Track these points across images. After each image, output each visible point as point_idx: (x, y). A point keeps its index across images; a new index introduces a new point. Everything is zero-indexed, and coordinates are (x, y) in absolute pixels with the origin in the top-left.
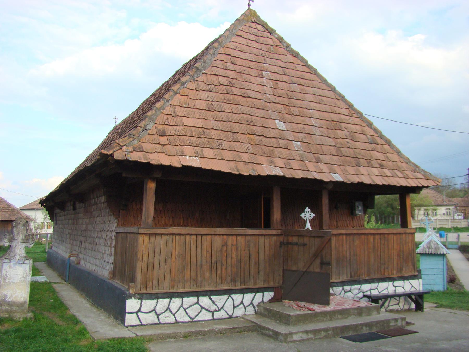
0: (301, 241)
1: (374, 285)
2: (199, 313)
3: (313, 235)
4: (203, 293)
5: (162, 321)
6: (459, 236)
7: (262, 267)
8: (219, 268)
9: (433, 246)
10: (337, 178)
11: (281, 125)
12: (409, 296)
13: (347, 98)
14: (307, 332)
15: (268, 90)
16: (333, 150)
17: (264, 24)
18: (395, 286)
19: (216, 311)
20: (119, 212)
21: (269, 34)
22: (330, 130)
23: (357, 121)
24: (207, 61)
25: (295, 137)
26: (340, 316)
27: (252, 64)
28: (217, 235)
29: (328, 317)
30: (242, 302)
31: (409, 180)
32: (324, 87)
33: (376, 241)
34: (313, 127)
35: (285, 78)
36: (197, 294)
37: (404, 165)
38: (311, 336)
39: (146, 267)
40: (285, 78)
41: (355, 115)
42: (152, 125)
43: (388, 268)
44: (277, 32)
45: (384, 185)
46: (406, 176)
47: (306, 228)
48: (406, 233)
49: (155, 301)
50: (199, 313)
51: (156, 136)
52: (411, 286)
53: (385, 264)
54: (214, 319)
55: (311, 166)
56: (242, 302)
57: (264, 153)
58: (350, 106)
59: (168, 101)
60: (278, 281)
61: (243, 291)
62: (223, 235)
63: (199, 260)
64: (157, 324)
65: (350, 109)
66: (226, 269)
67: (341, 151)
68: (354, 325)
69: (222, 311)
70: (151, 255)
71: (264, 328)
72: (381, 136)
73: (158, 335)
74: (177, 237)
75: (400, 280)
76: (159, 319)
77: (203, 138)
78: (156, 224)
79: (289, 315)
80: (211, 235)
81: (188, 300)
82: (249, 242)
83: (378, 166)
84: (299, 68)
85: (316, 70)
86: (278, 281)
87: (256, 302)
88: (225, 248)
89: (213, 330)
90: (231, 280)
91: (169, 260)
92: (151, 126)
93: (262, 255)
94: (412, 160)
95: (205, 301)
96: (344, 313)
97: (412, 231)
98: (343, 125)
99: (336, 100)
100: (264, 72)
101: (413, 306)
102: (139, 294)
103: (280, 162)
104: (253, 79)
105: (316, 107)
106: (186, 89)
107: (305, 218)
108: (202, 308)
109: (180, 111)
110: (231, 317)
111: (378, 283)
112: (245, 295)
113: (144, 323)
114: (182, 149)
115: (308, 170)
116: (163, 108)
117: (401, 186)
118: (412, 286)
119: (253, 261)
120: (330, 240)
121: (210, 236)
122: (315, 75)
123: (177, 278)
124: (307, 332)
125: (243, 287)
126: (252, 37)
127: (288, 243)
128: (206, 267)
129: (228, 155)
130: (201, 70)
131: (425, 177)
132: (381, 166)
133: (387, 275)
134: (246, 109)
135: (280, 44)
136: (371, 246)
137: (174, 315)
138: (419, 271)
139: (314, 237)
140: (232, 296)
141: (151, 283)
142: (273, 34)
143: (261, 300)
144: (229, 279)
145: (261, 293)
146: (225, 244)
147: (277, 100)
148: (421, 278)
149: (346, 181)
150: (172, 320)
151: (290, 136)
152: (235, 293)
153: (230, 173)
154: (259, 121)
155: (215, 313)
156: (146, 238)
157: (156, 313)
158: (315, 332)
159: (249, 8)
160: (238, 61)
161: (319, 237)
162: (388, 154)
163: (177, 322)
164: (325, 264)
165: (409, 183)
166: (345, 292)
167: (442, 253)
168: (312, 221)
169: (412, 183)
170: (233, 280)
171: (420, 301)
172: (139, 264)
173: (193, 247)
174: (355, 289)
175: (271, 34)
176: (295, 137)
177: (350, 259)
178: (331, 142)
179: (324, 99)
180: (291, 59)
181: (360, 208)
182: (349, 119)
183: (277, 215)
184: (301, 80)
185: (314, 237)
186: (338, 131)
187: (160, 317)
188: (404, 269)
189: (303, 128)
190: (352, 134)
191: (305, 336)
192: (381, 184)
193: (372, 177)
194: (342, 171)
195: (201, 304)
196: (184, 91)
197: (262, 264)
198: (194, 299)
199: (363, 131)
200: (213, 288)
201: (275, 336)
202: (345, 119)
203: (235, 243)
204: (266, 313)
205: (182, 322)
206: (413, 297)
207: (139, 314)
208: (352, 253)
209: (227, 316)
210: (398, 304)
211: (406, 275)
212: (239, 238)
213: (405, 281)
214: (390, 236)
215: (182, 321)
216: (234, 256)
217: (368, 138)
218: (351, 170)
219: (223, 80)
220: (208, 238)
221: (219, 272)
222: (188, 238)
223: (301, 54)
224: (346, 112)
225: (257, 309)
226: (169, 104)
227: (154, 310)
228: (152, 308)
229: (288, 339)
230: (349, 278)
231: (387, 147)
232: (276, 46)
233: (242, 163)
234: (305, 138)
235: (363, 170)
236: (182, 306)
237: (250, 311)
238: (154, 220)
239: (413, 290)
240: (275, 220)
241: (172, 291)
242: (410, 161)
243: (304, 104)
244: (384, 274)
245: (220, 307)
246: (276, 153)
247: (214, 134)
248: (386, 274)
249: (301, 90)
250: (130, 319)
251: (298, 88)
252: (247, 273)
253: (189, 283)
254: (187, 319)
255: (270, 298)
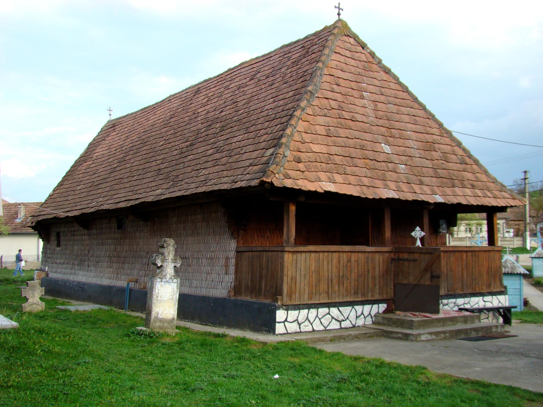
0: (411, 257)
1: (467, 300)
2: (330, 322)
3: (423, 251)
4: (333, 304)
5: (302, 330)
6: (517, 257)
7: (377, 282)
8: (345, 282)
9: (508, 264)
10: (439, 199)
11: (387, 149)
12: (496, 310)
13: (437, 117)
14: (431, 334)
15: (370, 112)
16: (431, 172)
17: (355, 37)
18: (484, 301)
19: (343, 321)
20: (239, 231)
21: (361, 48)
22: (426, 152)
23: (447, 140)
24: (318, 84)
25: (399, 160)
26: (450, 323)
27: (353, 85)
28: (343, 252)
29: (442, 324)
30: (362, 313)
31: (498, 200)
32: (416, 106)
33: (468, 258)
34: (412, 150)
35: (382, 98)
36: (328, 305)
37: (492, 185)
38: (434, 337)
39: (291, 281)
40: (382, 98)
41: (445, 135)
42: (289, 152)
43: (478, 284)
44: (368, 46)
45: (478, 205)
46: (495, 196)
47: (417, 245)
48: (493, 251)
49: (298, 311)
50: (330, 322)
51: (294, 163)
52: (498, 301)
53: (476, 280)
54: (341, 328)
55: (416, 188)
56: (362, 313)
57: (378, 176)
58: (440, 125)
59: (295, 128)
60: (391, 294)
61: (363, 303)
62: (348, 252)
63: (330, 274)
64: (299, 332)
65: (441, 129)
66: (350, 283)
67: (437, 173)
68: (465, 329)
69: (348, 321)
70: (294, 270)
71: (391, 332)
72: (470, 156)
73: (311, 339)
74: (313, 255)
75: (489, 296)
76: (300, 328)
77: (329, 164)
78: (297, 242)
79: (412, 321)
80: (339, 252)
81: (323, 311)
82: (368, 258)
83: (471, 187)
84: (393, 86)
85: (407, 88)
86: (391, 294)
87: (373, 313)
88: (349, 264)
89: (350, 335)
90: (354, 293)
91: (308, 275)
92: (288, 153)
93: (377, 270)
94: (499, 179)
95: (334, 311)
96: (453, 320)
97: (499, 249)
98: (436, 146)
99: (427, 120)
100: (364, 93)
101: (501, 320)
102: (285, 306)
103: (392, 185)
104: (357, 101)
105: (412, 128)
106: (306, 115)
107: (416, 236)
108: (333, 318)
109: (307, 138)
110: (354, 326)
111: (470, 297)
112: (365, 306)
113: (289, 332)
114: (318, 175)
115: (415, 193)
116: (292, 135)
117: (493, 206)
118: (500, 302)
119: (370, 276)
120: (439, 256)
121: (338, 253)
122: (406, 94)
123: (314, 292)
124: (431, 334)
125: (364, 299)
126: (348, 54)
127: (399, 259)
128: (335, 281)
129: (352, 179)
130: (314, 94)
131: (512, 196)
132: (473, 187)
133: (477, 290)
134: (357, 134)
135: (372, 60)
136: (464, 262)
137: (312, 324)
138: (505, 287)
139: (425, 253)
140: (355, 307)
141: (294, 296)
142: (365, 48)
143: (377, 311)
144: (352, 291)
145: (377, 305)
146: (349, 261)
147: (380, 122)
148: (507, 294)
149: (447, 202)
150: (309, 328)
151: (395, 159)
152: (357, 305)
153: (359, 197)
154: (369, 145)
155: (342, 323)
156: (290, 255)
157: (298, 322)
158: (437, 334)
159: (339, 17)
160: (341, 82)
161: (428, 253)
162: (477, 174)
163: (314, 330)
164: (435, 277)
165: (499, 203)
166: (444, 305)
167: (519, 272)
168: (422, 239)
169: (501, 203)
170: (356, 293)
171: (508, 315)
172: (285, 278)
173: (325, 263)
174: (452, 302)
175: (363, 48)
176: (399, 160)
177: (447, 275)
178: (428, 163)
179: (417, 118)
180: (385, 77)
181: (444, 226)
182: (441, 139)
183: (388, 234)
184: (396, 100)
185: (425, 253)
186: (433, 152)
187: (301, 326)
188: (492, 285)
189: (405, 150)
190: (445, 155)
191: (429, 337)
192: (475, 204)
193: (467, 197)
194: (441, 192)
195: (332, 314)
196: (304, 116)
197: (377, 279)
198: (326, 310)
199: (453, 151)
200: (341, 300)
201: (406, 337)
202: (438, 140)
203: (357, 259)
204: (384, 322)
205: (318, 331)
206: (501, 310)
207: (286, 323)
208: (448, 269)
209: (351, 326)
210: (487, 318)
211: (495, 290)
212: (360, 254)
213: (494, 297)
214: (480, 253)
215: (318, 329)
216: (356, 271)
217: (458, 158)
218: (448, 191)
219: (333, 104)
220: (336, 255)
221: (345, 286)
222: (321, 254)
223: (393, 70)
224: (436, 131)
225: (374, 319)
226: (295, 130)
227: (297, 320)
228: (295, 318)
229: (418, 339)
230: (446, 292)
231: (475, 167)
232: (370, 62)
233: (364, 187)
234: (408, 161)
235: (458, 191)
236: (317, 316)
237: (369, 321)
238: (295, 239)
239: (500, 305)
240: (386, 238)
241: (310, 302)
242: (497, 181)
243: (402, 125)
244: (475, 290)
245: (346, 317)
246: (387, 176)
247: (337, 159)
248: (477, 289)
249: (397, 110)
250: (279, 328)
251: (394, 108)
252: (366, 287)
253: (323, 295)
254: (322, 328)
255: (384, 309)
